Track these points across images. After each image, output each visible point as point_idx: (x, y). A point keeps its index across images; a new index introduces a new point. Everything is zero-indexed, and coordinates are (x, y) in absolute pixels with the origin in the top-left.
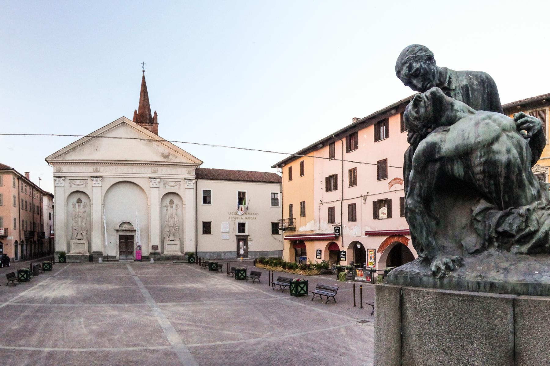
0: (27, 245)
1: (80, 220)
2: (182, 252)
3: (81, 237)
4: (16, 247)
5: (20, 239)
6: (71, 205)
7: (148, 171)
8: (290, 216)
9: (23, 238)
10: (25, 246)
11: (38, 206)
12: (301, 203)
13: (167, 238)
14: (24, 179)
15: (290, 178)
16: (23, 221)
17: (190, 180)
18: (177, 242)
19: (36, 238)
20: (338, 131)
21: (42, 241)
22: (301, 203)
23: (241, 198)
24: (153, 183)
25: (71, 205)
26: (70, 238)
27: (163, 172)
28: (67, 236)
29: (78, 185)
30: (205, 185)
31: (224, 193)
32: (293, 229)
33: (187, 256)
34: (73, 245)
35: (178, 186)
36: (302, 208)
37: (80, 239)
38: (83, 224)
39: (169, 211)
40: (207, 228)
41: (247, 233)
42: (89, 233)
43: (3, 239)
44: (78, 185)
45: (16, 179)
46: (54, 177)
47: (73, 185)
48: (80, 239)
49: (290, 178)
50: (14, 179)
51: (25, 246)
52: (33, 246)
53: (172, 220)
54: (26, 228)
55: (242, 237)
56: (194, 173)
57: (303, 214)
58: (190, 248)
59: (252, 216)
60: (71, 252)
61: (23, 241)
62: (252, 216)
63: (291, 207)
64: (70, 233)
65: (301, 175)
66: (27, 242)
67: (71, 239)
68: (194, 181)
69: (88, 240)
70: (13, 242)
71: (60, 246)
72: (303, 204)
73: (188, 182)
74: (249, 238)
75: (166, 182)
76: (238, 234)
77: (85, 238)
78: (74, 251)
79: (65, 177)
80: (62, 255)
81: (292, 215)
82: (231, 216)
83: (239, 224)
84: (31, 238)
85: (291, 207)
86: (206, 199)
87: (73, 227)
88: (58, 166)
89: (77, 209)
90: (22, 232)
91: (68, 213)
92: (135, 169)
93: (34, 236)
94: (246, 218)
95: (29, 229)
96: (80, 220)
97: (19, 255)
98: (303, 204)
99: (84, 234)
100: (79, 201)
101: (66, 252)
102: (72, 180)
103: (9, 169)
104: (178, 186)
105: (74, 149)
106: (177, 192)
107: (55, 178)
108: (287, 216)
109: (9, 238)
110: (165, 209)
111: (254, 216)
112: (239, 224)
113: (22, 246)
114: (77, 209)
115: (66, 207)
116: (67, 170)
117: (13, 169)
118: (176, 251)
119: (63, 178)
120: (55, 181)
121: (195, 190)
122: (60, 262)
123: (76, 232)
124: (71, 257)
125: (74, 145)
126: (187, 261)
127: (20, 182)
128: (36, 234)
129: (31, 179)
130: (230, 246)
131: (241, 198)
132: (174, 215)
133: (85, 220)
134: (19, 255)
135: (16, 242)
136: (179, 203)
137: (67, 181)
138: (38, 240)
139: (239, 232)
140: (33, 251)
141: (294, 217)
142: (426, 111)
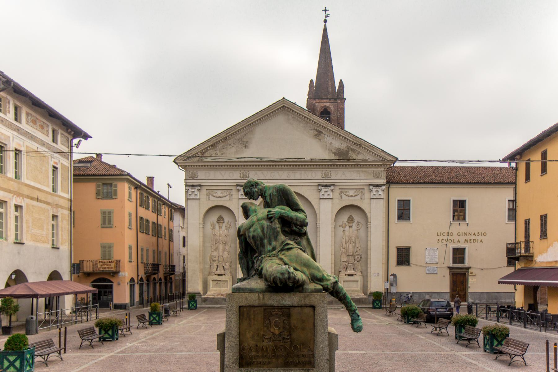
0: (148, 285)
1: (221, 246)
2: (365, 293)
3: (223, 272)
4: (132, 287)
5: (138, 276)
6: (208, 226)
7: (317, 176)
8: (525, 237)
9: (142, 274)
10: (145, 286)
11: (154, 223)
12: (541, 217)
13: (343, 273)
14: (146, 192)
15: (528, 178)
16: (142, 250)
17: (377, 186)
18: (358, 277)
19: (161, 275)
20: (540, 135)
21: (171, 279)
22: (541, 217)
23: (459, 207)
24: (326, 193)
25: (208, 226)
26: (207, 273)
27: (341, 177)
28: (202, 270)
29: (219, 197)
30: (399, 193)
31: (431, 204)
32: (529, 258)
33: (372, 299)
34: (211, 284)
35: (228, 197)
36: (542, 225)
37: (221, 275)
38: (226, 253)
39: (347, 233)
40: (404, 256)
41: (466, 264)
42: (233, 266)
43: (113, 276)
44: (219, 197)
45: (133, 188)
46: (186, 185)
47: (212, 198)
48: (221, 275)
49: (528, 178)
50: (130, 188)
51: (145, 286)
52: (158, 285)
53: (351, 245)
54: (147, 260)
55: (459, 271)
56: (383, 175)
57: (544, 234)
58: (377, 285)
59: (476, 237)
60: (208, 293)
61: (141, 278)
62: (476, 237)
63: (527, 222)
64: (208, 266)
65: (526, 180)
66: (148, 280)
67: (209, 274)
68: (384, 187)
69: (232, 275)
70: (128, 280)
71: (194, 285)
72: (544, 219)
73: (374, 189)
74: (470, 271)
75: (343, 190)
76: (451, 265)
77: (228, 272)
78: (213, 292)
79: (200, 186)
80: (193, 297)
81: (529, 236)
82: (441, 238)
83: (454, 249)
84: (154, 274)
85: (527, 222)
86: (404, 212)
87: (211, 257)
88: (191, 171)
89: (217, 231)
90: (141, 267)
91: (204, 237)
92: (298, 174)
93: (158, 270)
94: (466, 241)
95: (151, 261)
96: (221, 246)
97: (145, 298)
98: (544, 219)
99: (227, 266)
100: (220, 220)
101: (202, 294)
102: (211, 190)
103: (123, 175)
104: (360, 195)
105: (214, 146)
106: (359, 205)
107: (187, 188)
108: (521, 238)
109: (121, 274)
110: (342, 229)
111: (480, 238)
112: (454, 249)
113: (141, 286)
114: (217, 231)
115: (201, 230)
116: (203, 177)
117: (129, 175)
118: (356, 291)
119: (199, 188)
120: (187, 192)
121: (385, 201)
122: (189, 308)
123: (215, 265)
124: (205, 300)
125: (214, 141)
126: (371, 306)
127: (139, 192)
128: (161, 269)
129: (160, 193)
130: (442, 285)
131: (459, 207)
132: (353, 239)
133: (228, 247)
134: (137, 299)
135: (132, 280)
136: (362, 221)
137: (204, 192)
138: (165, 278)
139: (454, 262)
140: (145, 294)
141: (531, 240)
142: (349, 233)
